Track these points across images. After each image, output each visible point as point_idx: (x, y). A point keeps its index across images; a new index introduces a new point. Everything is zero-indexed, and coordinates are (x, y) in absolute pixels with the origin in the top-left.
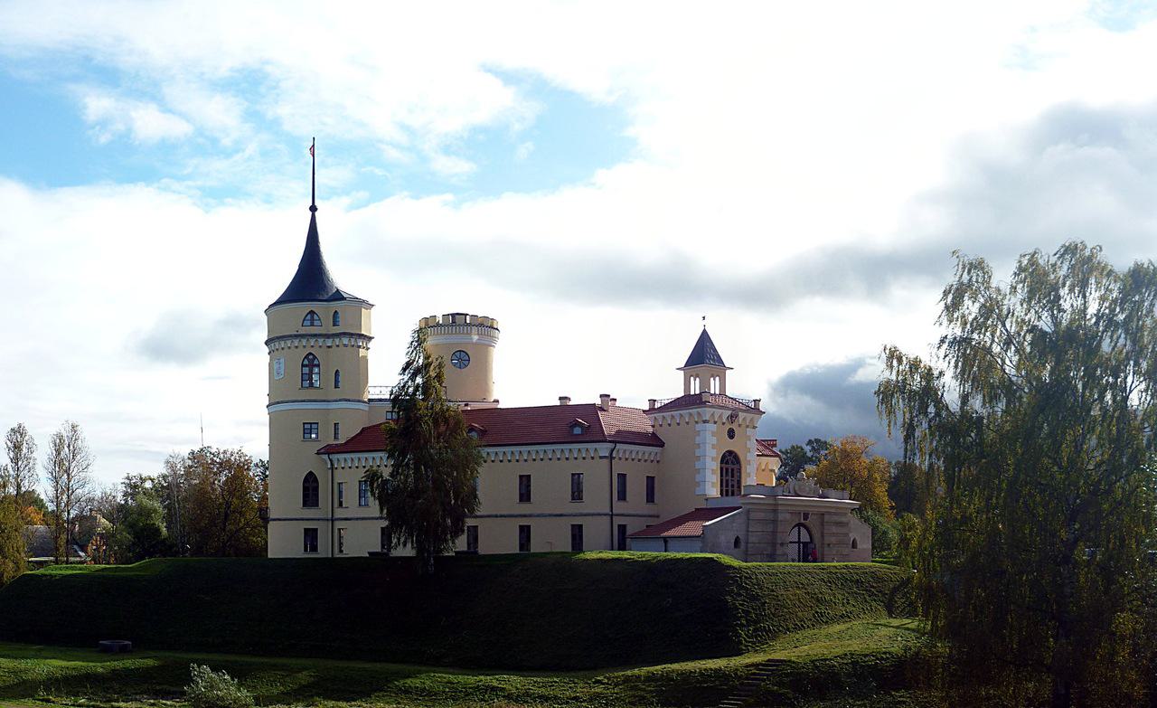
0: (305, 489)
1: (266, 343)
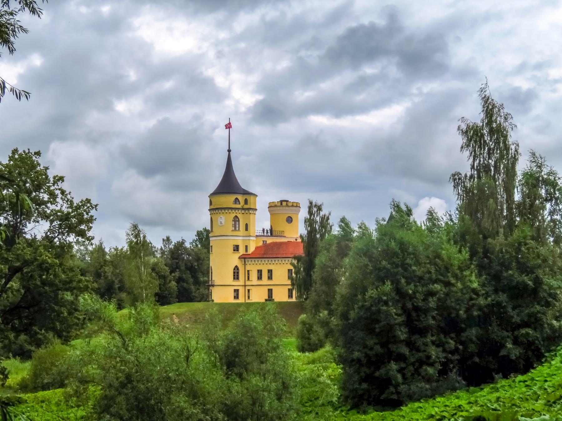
0: (234, 273)
1: (210, 210)
